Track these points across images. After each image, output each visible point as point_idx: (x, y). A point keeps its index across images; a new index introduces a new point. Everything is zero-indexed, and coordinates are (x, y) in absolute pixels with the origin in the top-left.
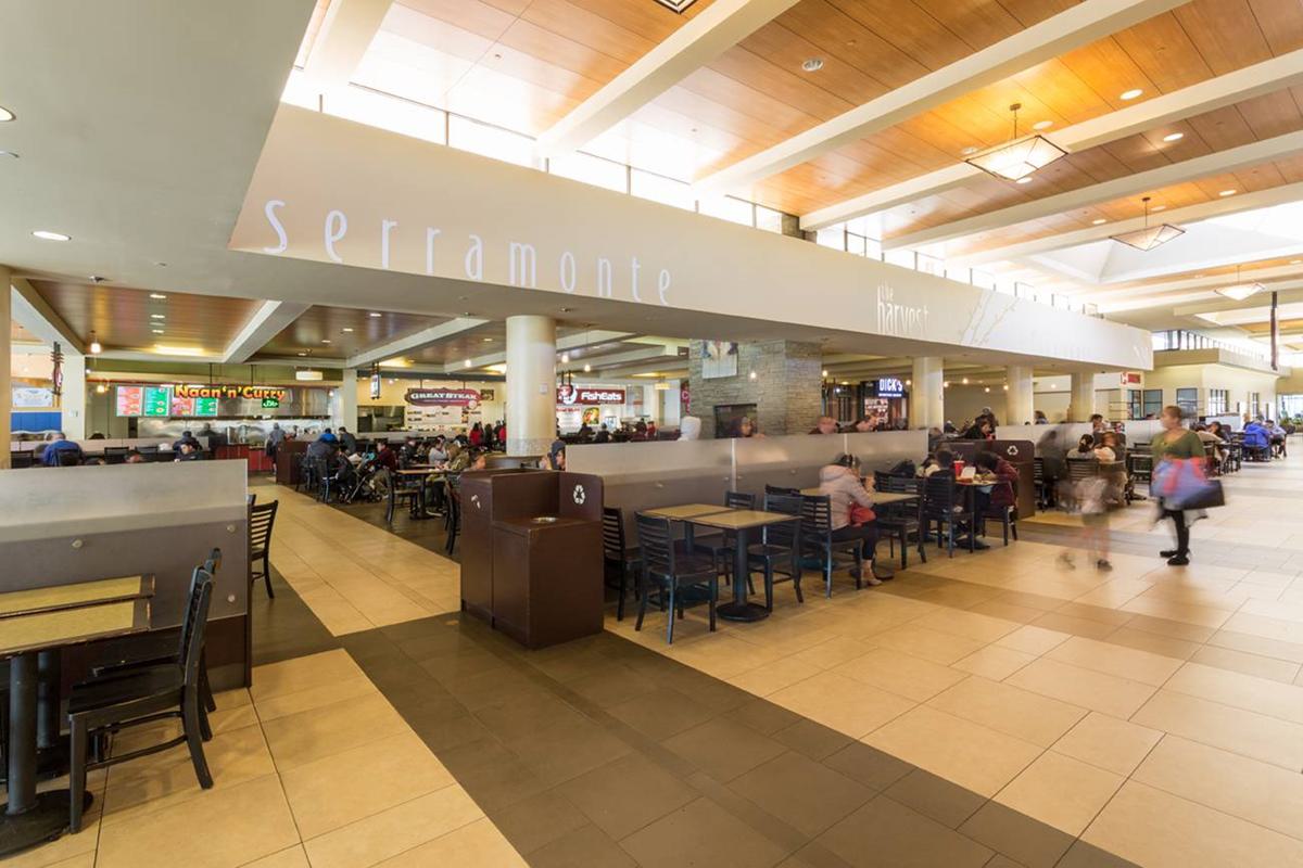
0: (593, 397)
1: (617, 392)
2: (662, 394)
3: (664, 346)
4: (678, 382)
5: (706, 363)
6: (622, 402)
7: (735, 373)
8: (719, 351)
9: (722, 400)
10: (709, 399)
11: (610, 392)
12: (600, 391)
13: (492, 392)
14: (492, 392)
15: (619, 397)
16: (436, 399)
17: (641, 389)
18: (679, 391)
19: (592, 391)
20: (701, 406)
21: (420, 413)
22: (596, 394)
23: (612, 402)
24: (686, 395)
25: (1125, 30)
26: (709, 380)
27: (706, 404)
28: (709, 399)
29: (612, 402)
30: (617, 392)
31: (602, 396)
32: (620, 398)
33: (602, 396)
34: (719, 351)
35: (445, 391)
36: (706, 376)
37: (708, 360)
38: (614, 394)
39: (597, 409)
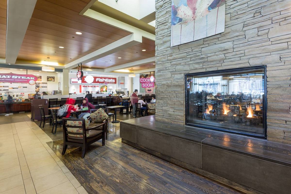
0: (101, 80)
1: (113, 79)
2: (132, 79)
3: (131, 33)
4: (139, 75)
5: (176, 30)
6: (115, 83)
7: (221, 29)
8: (194, 10)
9: (197, 66)
10: (178, 67)
11: (110, 78)
12: (105, 78)
13: (54, 78)
14: (54, 78)
15: (114, 81)
16: (5, 79)
17: (123, 78)
18: (139, 78)
19: (101, 78)
20: (169, 75)
21: (8, 87)
22: (103, 79)
23: (110, 83)
24: (142, 80)
25: (226, 11)
26: (179, 47)
27: (173, 73)
28: (178, 67)
29: (110, 83)
30: (113, 79)
31: (106, 80)
32: (114, 81)
33: (106, 80)
34: (194, 10)
35: (12, 74)
36: (175, 42)
37: (178, 26)
38: (111, 80)
39: (107, 86)
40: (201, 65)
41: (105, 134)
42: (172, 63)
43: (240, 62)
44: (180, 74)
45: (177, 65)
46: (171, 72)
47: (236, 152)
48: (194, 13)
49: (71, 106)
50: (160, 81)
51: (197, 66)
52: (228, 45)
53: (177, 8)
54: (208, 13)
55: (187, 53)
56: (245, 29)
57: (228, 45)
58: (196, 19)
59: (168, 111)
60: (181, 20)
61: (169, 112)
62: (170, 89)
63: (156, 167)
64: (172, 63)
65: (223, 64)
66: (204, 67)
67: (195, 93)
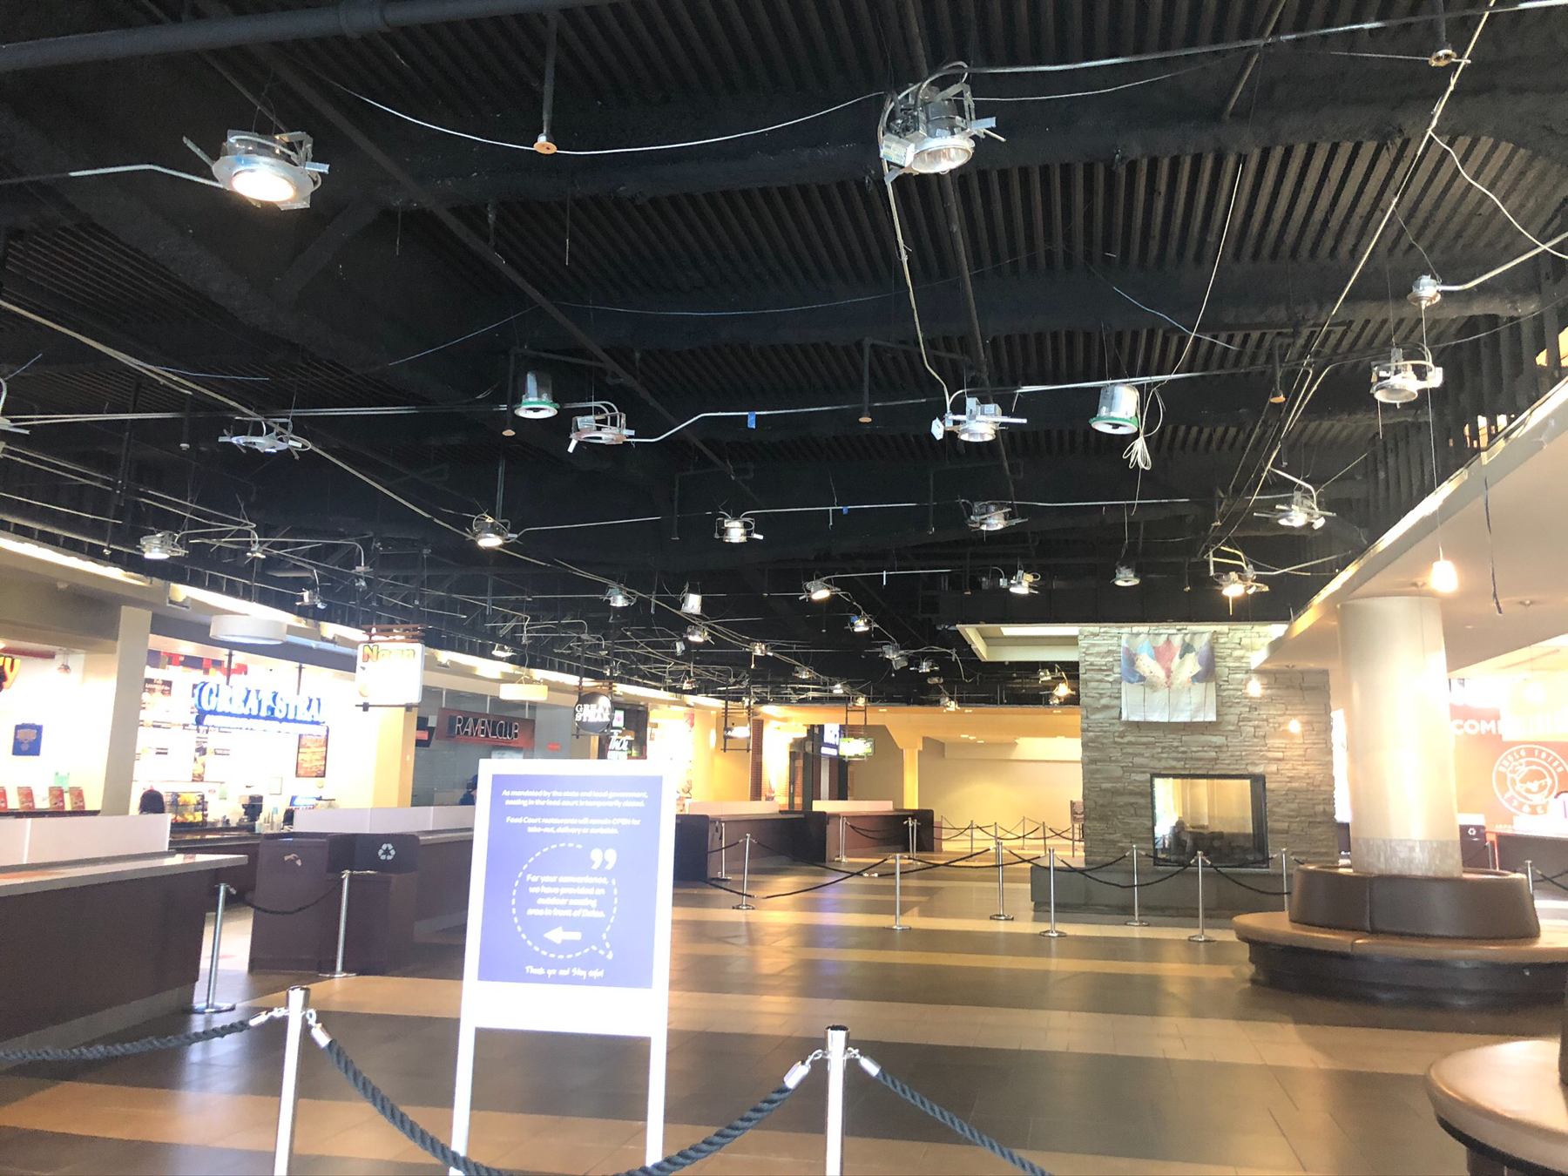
20: (1119, 772)
26: (1138, 725)
40: (1183, 763)
41: (763, 411)
42: (1125, 751)
43: (1237, 767)
44: (1144, 772)
45: (1136, 755)
46: (1122, 767)
47: (549, 630)
48: (1168, 676)
49: (1213, 553)
50: (378, 653)
51: (1174, 763)
52: (1218, 740)
53: (1135, 655)
54: (1190, 684)
55: (221, 730)
56: (1241, 724)
57: (1218, 740)
58: (1174, 687)
59: (1119, 842)
60: (1142, 678)
61: (1121, 845)
62: (1121, 800)
63: (468, 404)
64: (1125, 751)
65: (1216, 767)
66: (1187, 766)
67: (869, 744)
